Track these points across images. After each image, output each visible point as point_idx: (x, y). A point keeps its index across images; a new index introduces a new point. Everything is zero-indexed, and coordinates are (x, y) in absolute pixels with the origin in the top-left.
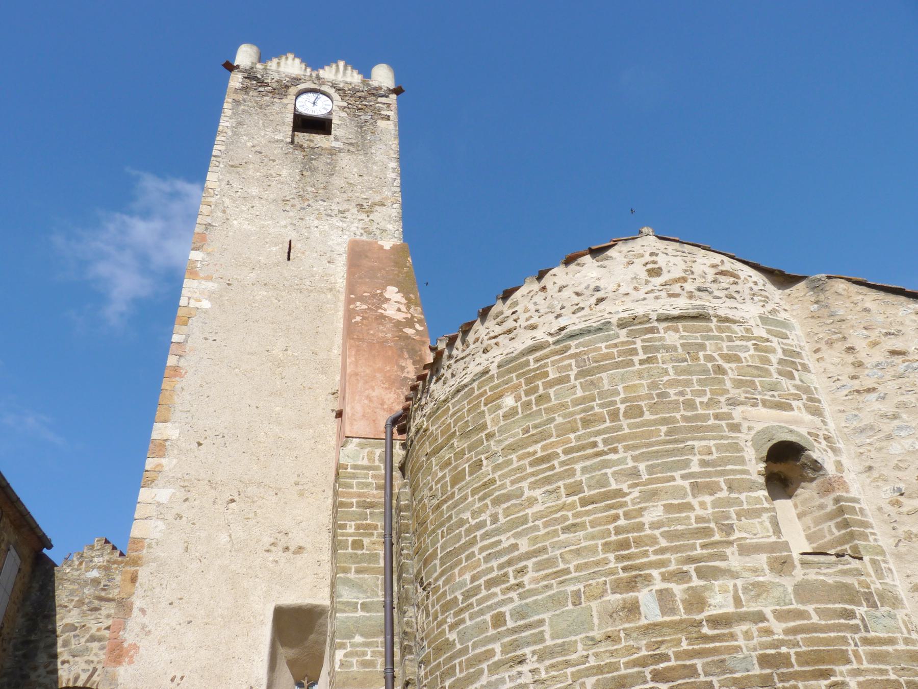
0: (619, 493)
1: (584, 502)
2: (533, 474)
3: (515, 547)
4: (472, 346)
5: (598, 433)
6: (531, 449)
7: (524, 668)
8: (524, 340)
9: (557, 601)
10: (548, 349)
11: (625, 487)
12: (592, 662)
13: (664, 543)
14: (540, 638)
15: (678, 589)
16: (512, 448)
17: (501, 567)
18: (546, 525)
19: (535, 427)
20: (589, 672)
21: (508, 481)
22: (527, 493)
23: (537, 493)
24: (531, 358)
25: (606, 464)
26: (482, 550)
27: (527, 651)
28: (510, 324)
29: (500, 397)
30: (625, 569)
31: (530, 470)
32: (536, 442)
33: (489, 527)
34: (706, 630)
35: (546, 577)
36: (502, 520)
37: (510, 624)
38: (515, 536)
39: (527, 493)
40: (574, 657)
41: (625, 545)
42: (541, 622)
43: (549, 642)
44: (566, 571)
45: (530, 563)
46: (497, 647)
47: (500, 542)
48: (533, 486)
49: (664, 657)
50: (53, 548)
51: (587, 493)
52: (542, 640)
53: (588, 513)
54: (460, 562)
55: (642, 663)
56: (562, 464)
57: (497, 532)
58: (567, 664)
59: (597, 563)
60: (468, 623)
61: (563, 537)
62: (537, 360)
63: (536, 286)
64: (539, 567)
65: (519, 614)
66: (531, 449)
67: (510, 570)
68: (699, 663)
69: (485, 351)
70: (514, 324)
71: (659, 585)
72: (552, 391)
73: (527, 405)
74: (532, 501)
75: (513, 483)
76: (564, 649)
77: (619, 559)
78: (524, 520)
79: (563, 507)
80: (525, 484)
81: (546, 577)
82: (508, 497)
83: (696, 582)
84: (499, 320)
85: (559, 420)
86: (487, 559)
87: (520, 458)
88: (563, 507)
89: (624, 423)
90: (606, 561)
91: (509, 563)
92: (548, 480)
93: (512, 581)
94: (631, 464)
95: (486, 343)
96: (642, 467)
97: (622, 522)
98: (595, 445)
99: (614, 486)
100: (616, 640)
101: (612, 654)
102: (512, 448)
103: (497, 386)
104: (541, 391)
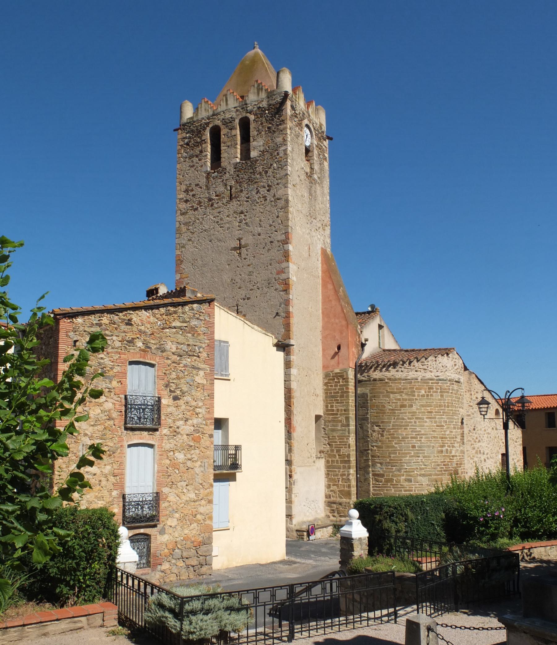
0: (443, 426)
1: (437, 426)
2: (427, 415)
3: (420, 431)
4: (412, 367)
5: (442, 410)
6: (427, 408)
7: (419, 458)
8: (428, 375)
9: (429, 446)
10: (434, 381)
11: (444, 424)
12: (434, 460)
13: (448, 439)
14: (424, 453)
15: (449, 449)
16: (423, 406)
17: (416, 435)
18: (429, 429)
19: (429, 403)
20: (433, 462)
21: (420, 414)
22: (425, 419)
23: (427, 420)
24: (430, 381)
25: (442, 418)
26: (410, 429)
27: (421, 455)
28: (425, 367)
29: (421, 389)
30: (442, 443)
31: (426, 414)
32: (429, 407)
33: (413, 424)
34: (451, 458)
35: (427, 441)
36: (418, 424)
37: (417, 448)
38: (421, 429)
39: (425, 419)
40: (430, 459)
41: (442, 438)
42: (425, 450)
43: (426, 455)
44: (432, 441)
45: (424, 436)
46: (412, 452)
47: (416, 429)
48: (427, 418)
49: (445, 462)
50: (9, 275)
51: (438, 424)
52: (424, 454)
53: (437, 429)
54: (402, 429)
55: (442, 462)
56: (434, 415)
57: (416, 426)
58: (429, 460)
59: (438, 441)
60: (403, 444)
61: (432, 433)
62: (432, 383)
63: (434, 359)
64: (426, 438)
65: (419, 447)
66: (427, 408)
67: (418, 436)
68: (449, 463)
69: (416, 371)
70: (427, 368)
71: (447, 448)
72: (434, 394)
73: (428, 395)
74: (426, 422)
75: (422, 415)
76: (429, 457)
77: (442, 441)
78: (424, 426)
79: (433, 426)
80: (425, 417)
81: (427, 441)
82: (420, 418)
83: (451, 448)
84: (422, 364)
85: (435, 403)
86: (412, 431)
87: (424, 410)
88: (433, 426)
89: (446, 409)
90: (439, 441)
91: (418, 435)
92: (430, 418)
93: (419, 439)
94: (446, 420)
95: (417, 369)
96: (448, 420)
97: (443, 433)
98: (440, 412)
99: (443, 424)
100: (439, 457)
101: (438, 459)
102: (423, 406)
103: (420, 385)
104: (432, 393)
